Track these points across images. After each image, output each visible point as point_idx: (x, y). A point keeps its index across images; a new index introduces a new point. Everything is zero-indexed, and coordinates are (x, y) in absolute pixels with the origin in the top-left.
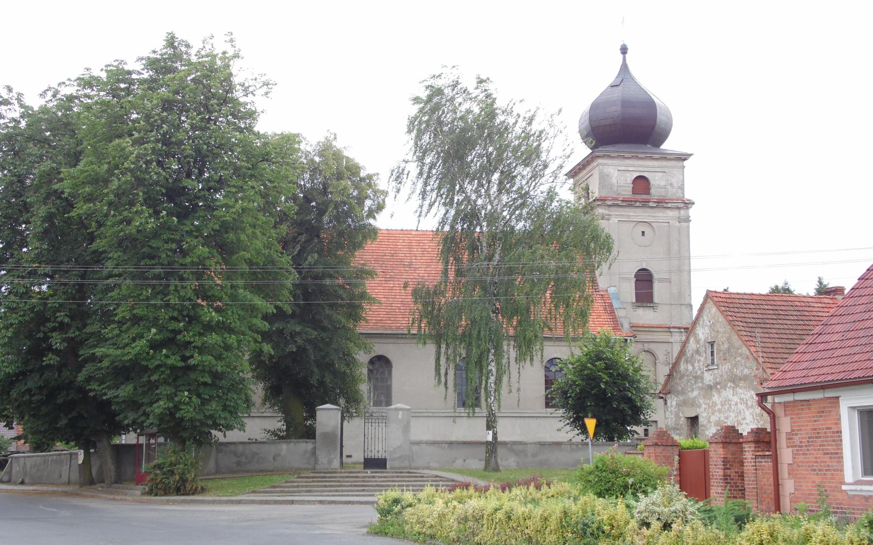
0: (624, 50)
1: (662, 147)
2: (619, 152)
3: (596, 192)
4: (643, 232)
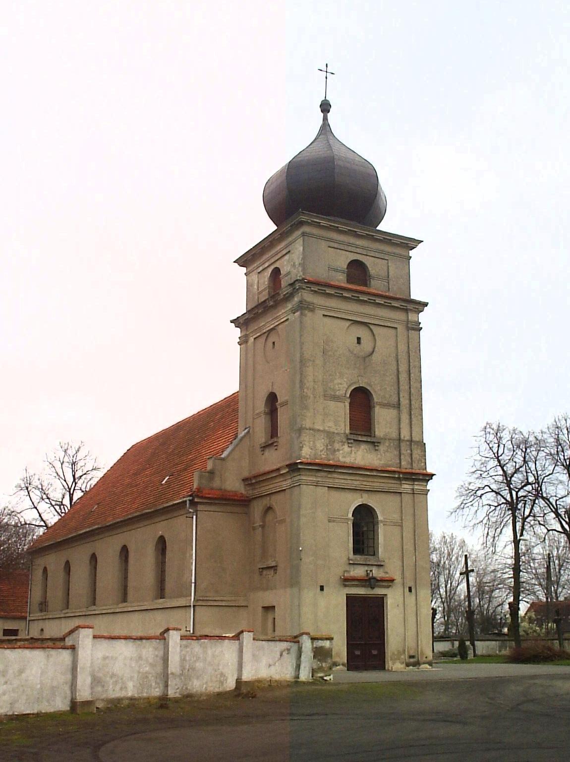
0: (325, 107)
1: (380, 227)
2: (334, 222)
3: (535, 505)
4: (359, 339)
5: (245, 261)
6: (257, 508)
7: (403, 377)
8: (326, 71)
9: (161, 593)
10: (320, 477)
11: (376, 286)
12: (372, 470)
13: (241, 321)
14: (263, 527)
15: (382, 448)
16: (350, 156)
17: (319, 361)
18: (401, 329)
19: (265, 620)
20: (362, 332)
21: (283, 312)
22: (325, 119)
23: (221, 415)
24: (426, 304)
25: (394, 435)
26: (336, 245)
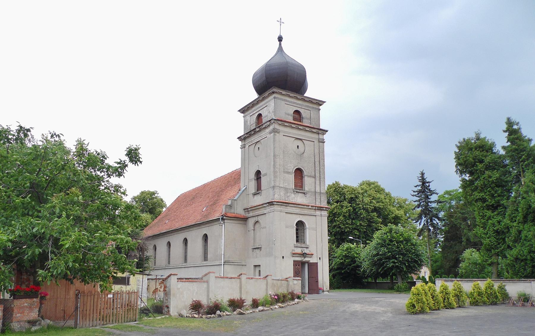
0: (280, 39)
4: (298, 146)
5: (243, 111)
6: (251, 222)
7: (317, 163)
8: (281, 22)
9: (206, 258)
10: (283, 208)
11: (306, 123)
12: (299, 204)
13: (242, 138)
14: (254, 230)
15: (308, 195)
16: (294, 62)
17: (281, 157)
18: (316, 142)
19: (255, 271)
20: (299, 143)
21: (265, 133)
22: (280, 44)
23: (233, 179)
24: (327, 131)
25: (313, 190)
26: (288, 103)
